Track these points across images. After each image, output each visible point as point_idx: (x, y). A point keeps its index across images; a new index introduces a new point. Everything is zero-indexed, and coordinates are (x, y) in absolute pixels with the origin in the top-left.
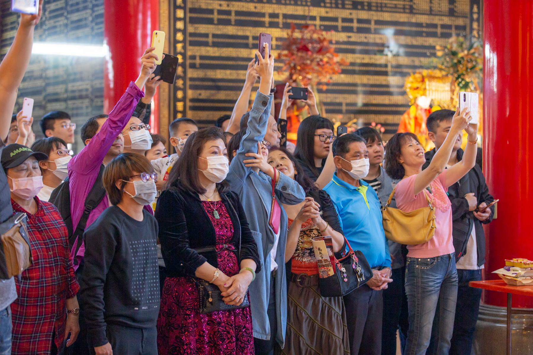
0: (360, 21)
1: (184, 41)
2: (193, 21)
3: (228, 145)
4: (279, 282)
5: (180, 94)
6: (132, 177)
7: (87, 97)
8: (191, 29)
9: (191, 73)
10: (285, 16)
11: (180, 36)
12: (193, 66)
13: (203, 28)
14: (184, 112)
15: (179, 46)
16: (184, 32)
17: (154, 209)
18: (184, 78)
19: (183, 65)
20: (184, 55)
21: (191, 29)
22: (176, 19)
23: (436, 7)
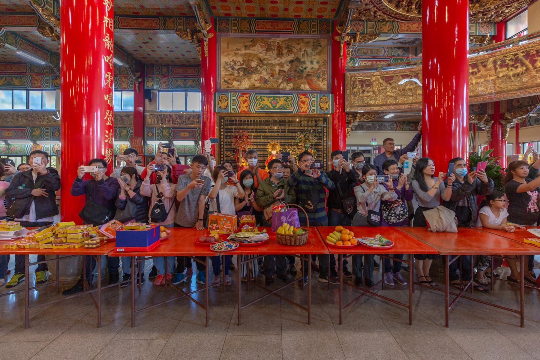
0: (282, 129)
1: (224, 138)
2: (226, 132)
3: (213, 171)
4: (91, 142)
5: (222, 153)
6: (39, 175)
7: (34, 319)
8: (226, 134)
9: (225, 147)
10: (256, 129)
11: (222, 137)
12: (226, 145)
13: (229, 134)
14: (223, 158)
15: (222, 140)
16: (224, 135)
17: (537, 277)
18: (223, 148)
19: (223, 145)
20: (223, 142)
21: (226, 134)
22: (221, 132)
23: (310, 124)
